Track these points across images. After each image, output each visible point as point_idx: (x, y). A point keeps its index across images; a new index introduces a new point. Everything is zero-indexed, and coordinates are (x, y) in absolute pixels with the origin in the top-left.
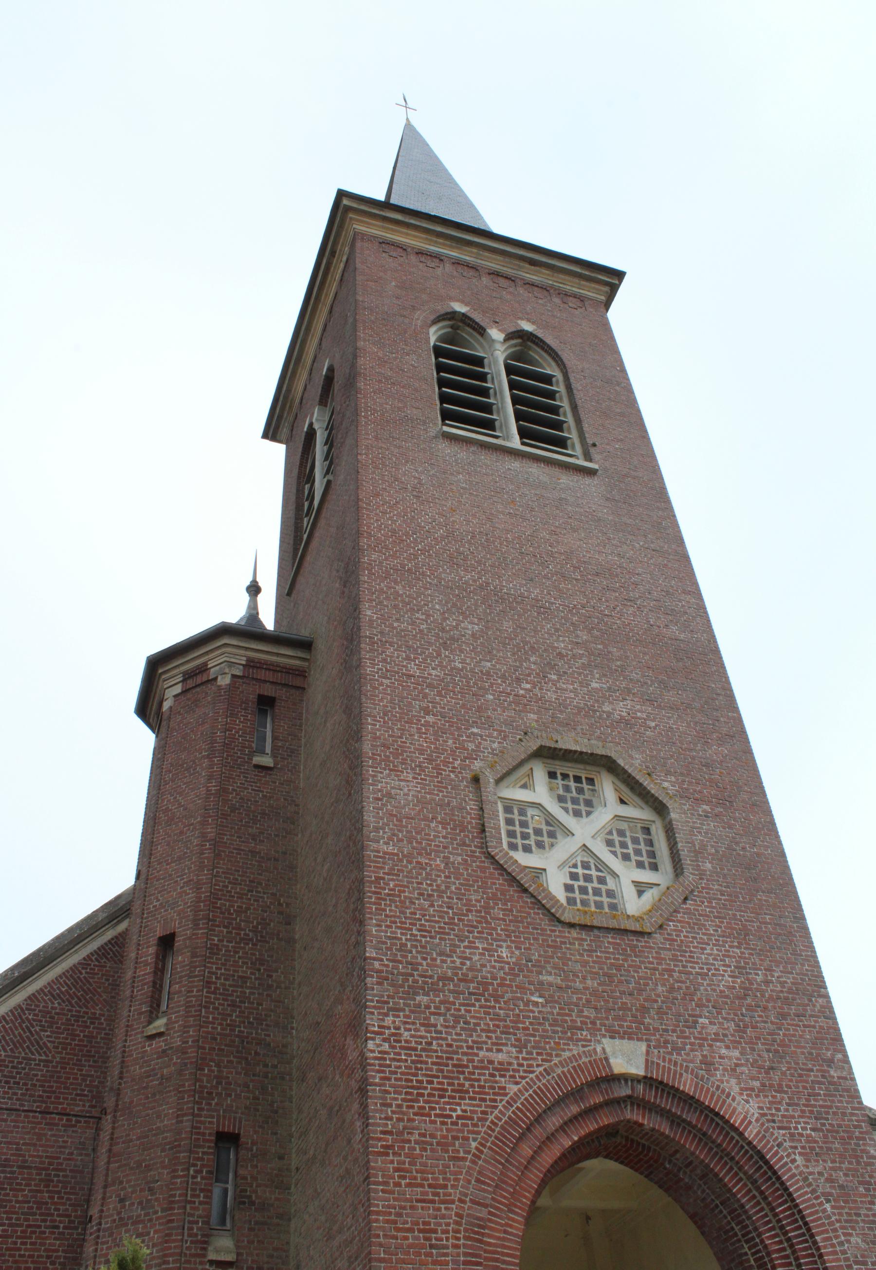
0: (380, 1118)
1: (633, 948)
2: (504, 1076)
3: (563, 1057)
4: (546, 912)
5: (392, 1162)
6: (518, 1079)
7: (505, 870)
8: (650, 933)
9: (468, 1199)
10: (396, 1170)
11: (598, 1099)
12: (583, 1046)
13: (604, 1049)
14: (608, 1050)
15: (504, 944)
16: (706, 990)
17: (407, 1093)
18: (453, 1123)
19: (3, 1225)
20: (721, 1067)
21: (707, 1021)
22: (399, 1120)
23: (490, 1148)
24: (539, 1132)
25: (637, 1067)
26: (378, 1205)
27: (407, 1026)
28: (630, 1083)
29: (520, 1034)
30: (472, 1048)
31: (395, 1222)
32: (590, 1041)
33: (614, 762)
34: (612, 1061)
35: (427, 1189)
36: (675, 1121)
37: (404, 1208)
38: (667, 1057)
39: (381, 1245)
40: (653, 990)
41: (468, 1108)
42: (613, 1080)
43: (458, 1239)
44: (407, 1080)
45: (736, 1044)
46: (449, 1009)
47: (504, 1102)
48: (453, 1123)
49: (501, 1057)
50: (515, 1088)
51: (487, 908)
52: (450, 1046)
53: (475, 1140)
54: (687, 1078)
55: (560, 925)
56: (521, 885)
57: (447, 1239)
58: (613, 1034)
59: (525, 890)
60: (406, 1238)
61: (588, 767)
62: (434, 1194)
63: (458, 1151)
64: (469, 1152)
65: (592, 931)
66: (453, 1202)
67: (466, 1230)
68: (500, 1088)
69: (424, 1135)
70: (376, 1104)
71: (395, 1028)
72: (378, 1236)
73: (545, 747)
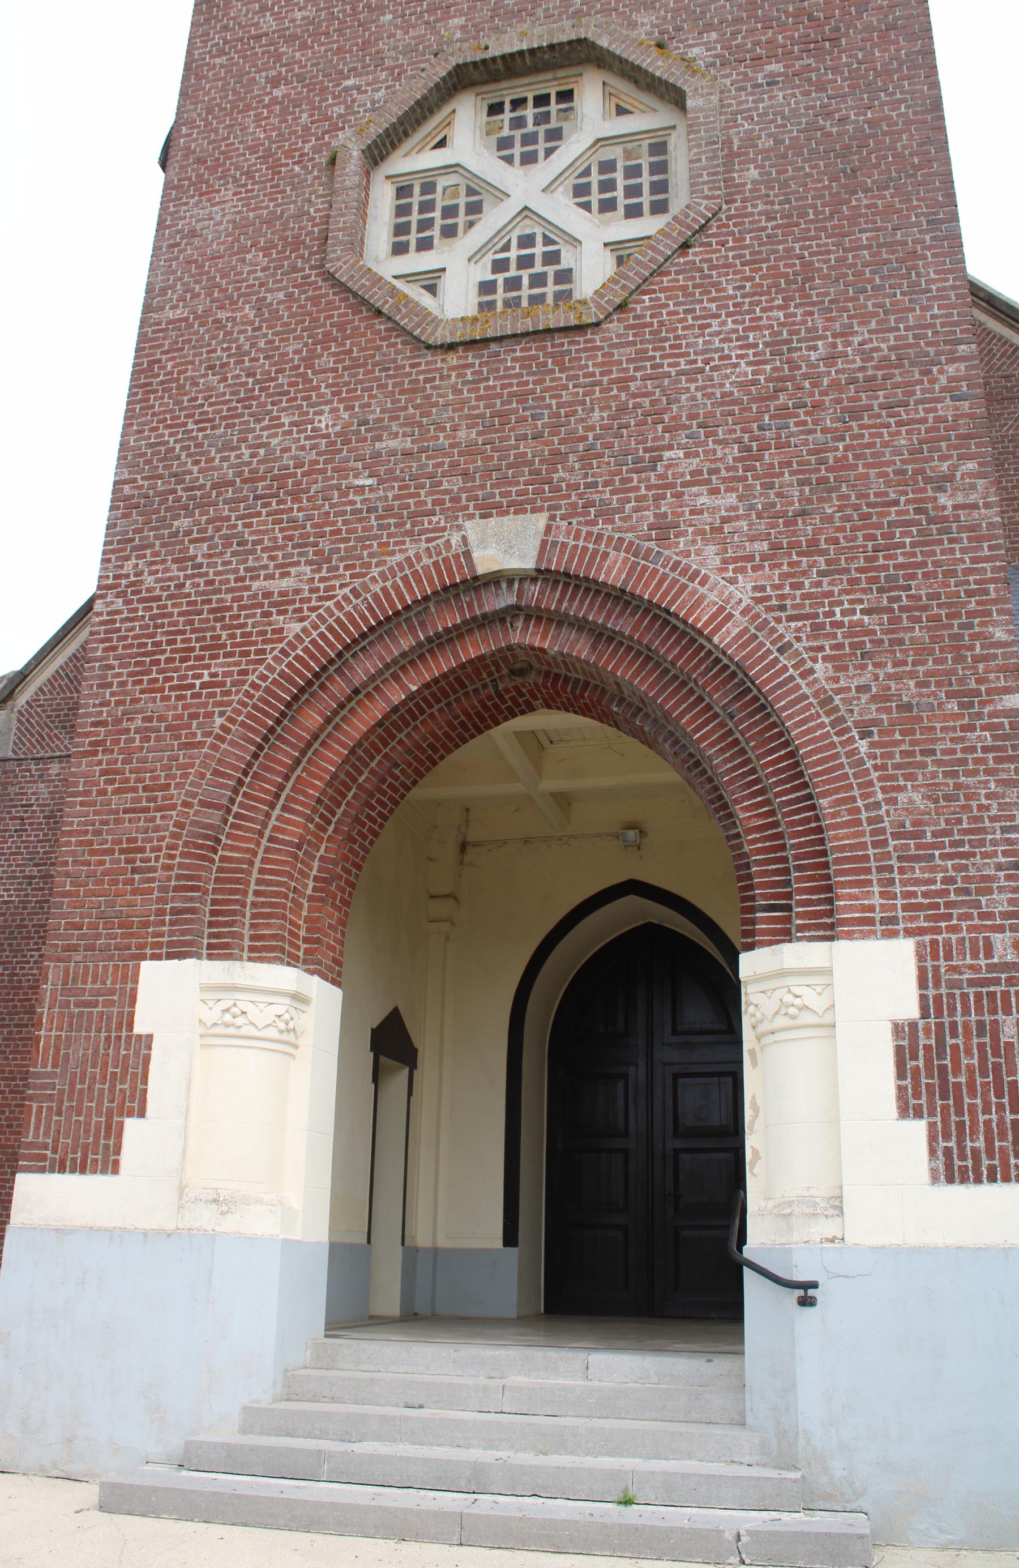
0: (95, 706)
1: (559, 359)
2: (284, 612)
3: (389, 564)
4: (409, 338)
5: (100, 763)
6: (306, 613)
7: (349, 290)
8: (597, 324)
9: (196, 801)
10: (103, 773)
11: (453, 619)
12: (429, 540)
13: (464, 538)
14: (472, 538)
15: (327, 408)
16: (693, 398)
17: (137, 664)
18: (194, 696)
19: (2, 866)
20: (691, 530)
21: (681, 453)
22: (118, 703)
23: (243, 724)
24: (339, 688)
25: (523, 557)
26: (72, 824)
27: (154, 568)
28: (516, 586)
29: (325, 545)
30: (242, 579)
31: (90, 843)
32: (444, 529)
33: (593, 46)
34: (475, 555)
35: (141, 793)
36: (600, 636)
37: (105, 823)
38: (585, 529)
39: (67, 875)
40: (582, 420)
41: (220, 670)
42: (486, 585)
43: (172, 857)
44: (141, 645)
45: (731, 483)
46: (218, 529)
47: (276, 652)
48: (194, 696)
49: (286, 584)
50: (297, 627)
51: (308, 362)
52: (211, 582)
53: (222, 714)
54: (617, 558)
55: (429, 353)
56: (370, 307)
57: (157, 858)
58: (487, 510)
59: (379, 313)
60: (102, 863)
61: (561, 73)
62: (149, 800)
63: (194, 735)
64: (208, 734)
65: (487, 347)
66: (173, 807)
67: (186, 844)
68: (274, 632)
69: (149, 719)
70: (92, 686)
71: (136, 575)
72: (66, 863)
73: (465, 65)
